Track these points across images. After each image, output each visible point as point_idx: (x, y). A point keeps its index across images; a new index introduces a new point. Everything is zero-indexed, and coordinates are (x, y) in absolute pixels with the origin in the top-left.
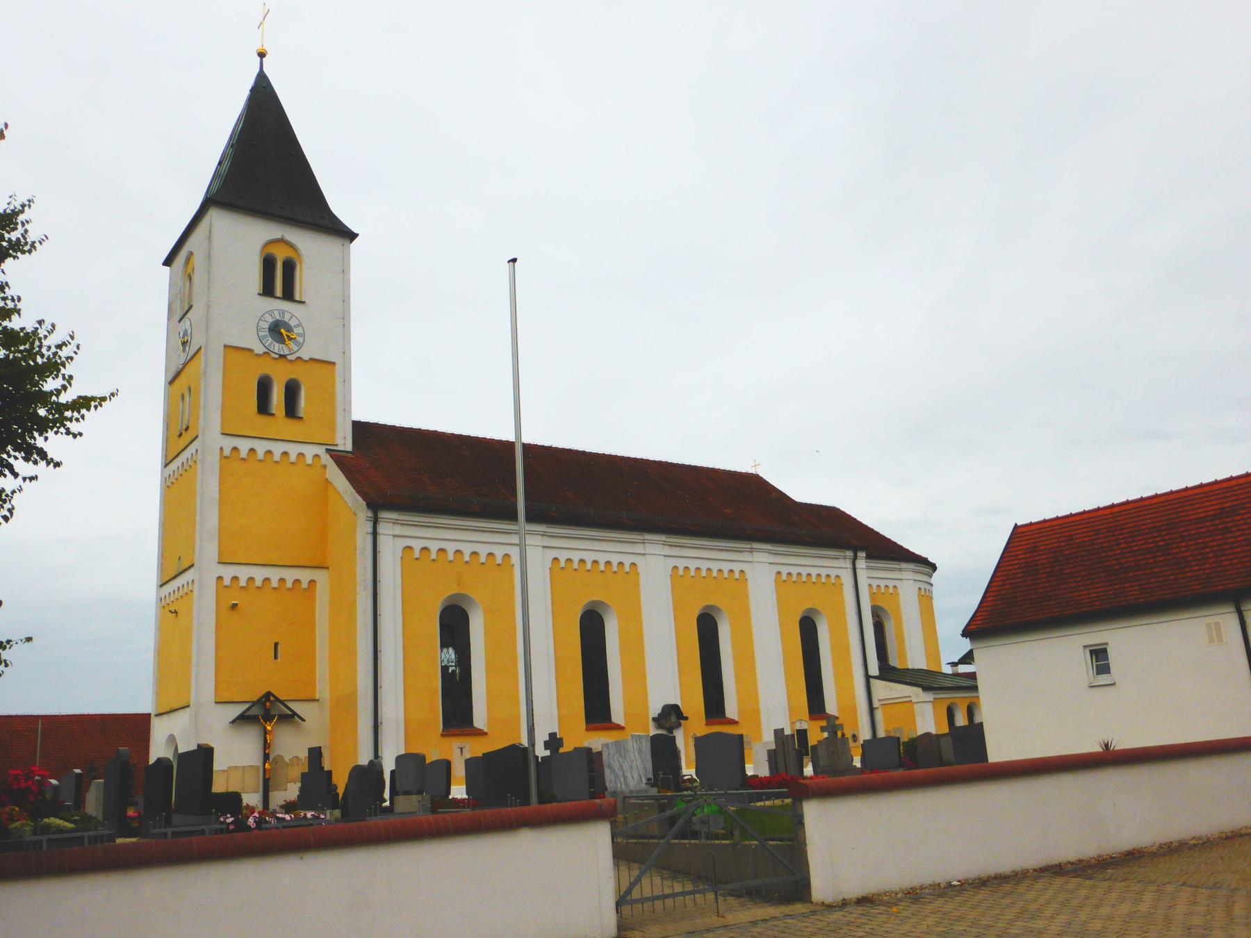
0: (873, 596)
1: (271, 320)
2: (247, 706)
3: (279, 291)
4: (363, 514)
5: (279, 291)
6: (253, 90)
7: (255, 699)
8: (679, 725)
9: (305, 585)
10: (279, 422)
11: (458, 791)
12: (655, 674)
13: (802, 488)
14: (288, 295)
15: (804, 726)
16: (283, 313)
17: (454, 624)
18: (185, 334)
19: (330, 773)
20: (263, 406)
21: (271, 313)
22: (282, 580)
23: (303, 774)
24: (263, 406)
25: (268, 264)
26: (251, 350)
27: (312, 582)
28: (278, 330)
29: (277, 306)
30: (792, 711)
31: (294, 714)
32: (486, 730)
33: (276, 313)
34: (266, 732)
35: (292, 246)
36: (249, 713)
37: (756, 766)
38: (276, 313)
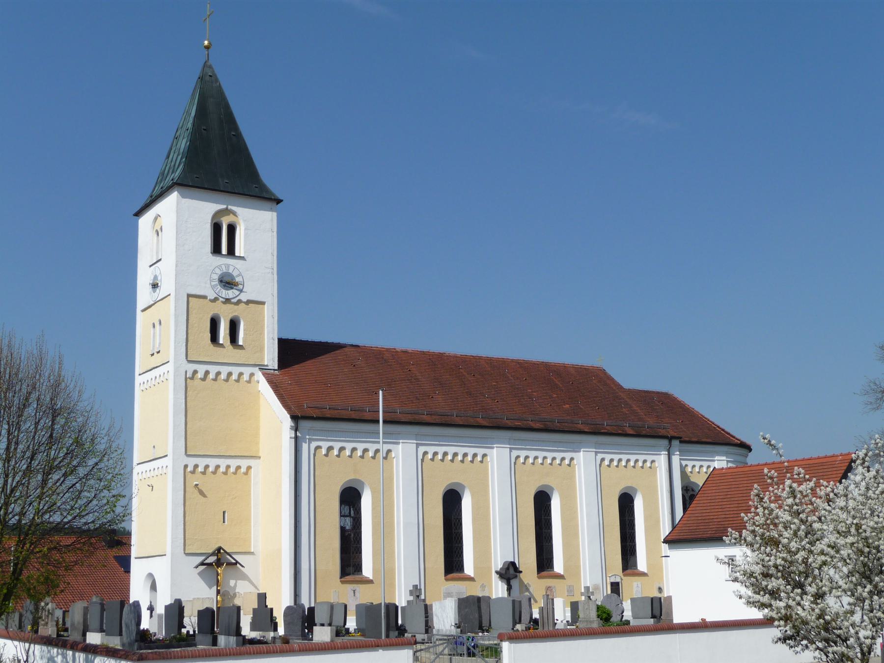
0: (684, 474)
1: (219, 272)
2: (203, 558)
3: (224, 250)
4: (287, 421)
5: (224, 250)
6: (201, 78)
7: (211, 551)
8: (516, 577)
9: (243, 470)
10: (228, 352)
11: (352, 624)
12: (495, 536)
13: (632, 376)
14: (231, 251)
15: (618, 580)
16: (228, 266)
17: (350, 498)
18: (156, 277)
19: (272, 610)
20: (214, 338)
21: (219, 267)
22: (228, 467)
23: (254, 610)
24: (214, 338)
25: (216, 229)
26: (205, 297)
27: (249, 468)
28: (227, 282)
29: (223, 263)
30: (605, 569)
31: (237, 562)
32: (371, 578)
33: (223, 267)
34: (218, 574)
35: (234, 214)
36: (206, 562)
37: (814, 479)
38: (223, 267)
